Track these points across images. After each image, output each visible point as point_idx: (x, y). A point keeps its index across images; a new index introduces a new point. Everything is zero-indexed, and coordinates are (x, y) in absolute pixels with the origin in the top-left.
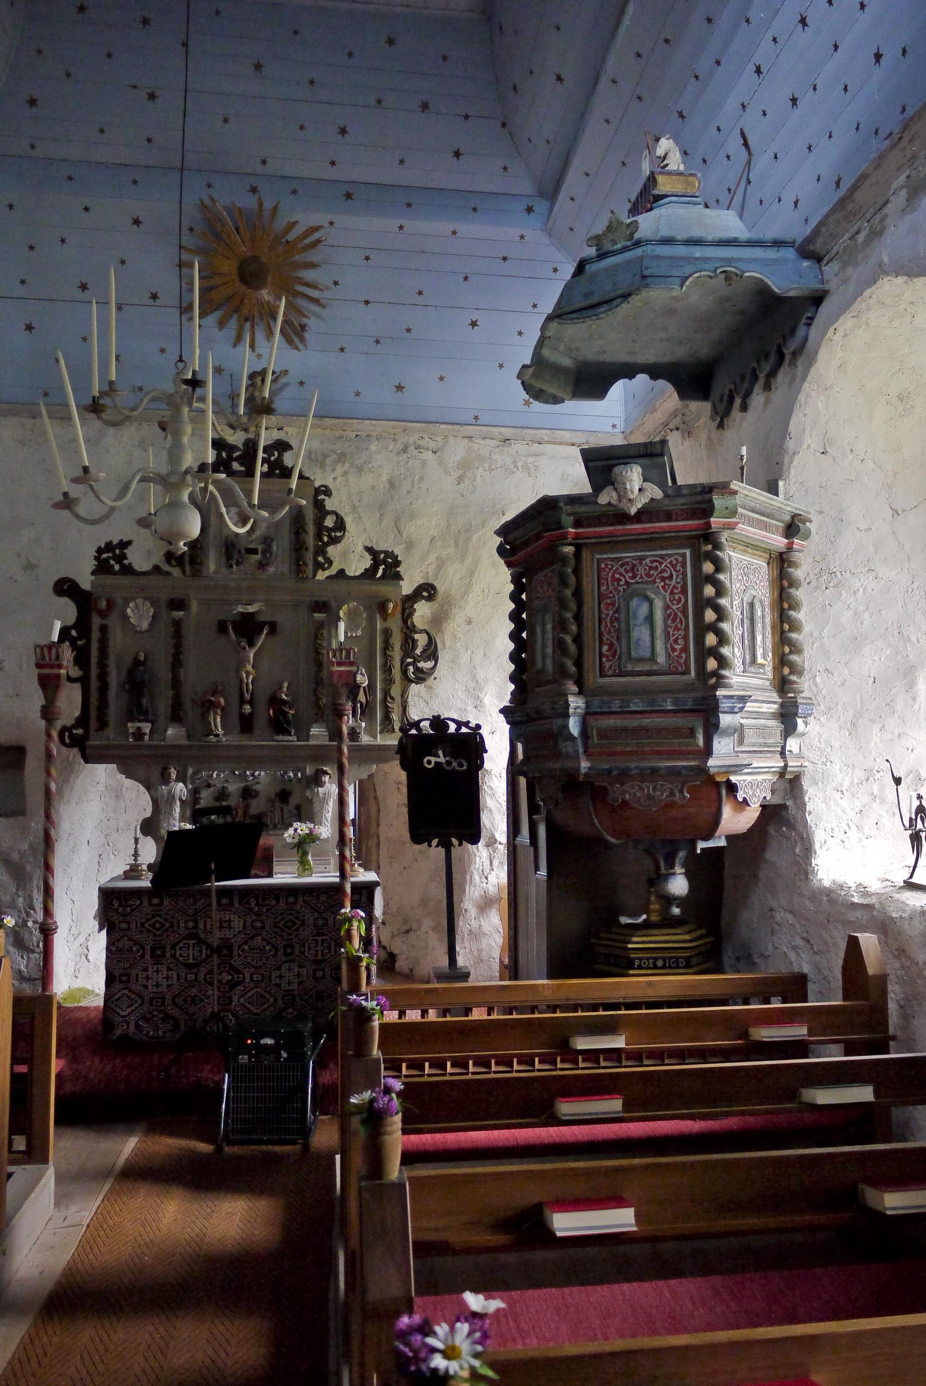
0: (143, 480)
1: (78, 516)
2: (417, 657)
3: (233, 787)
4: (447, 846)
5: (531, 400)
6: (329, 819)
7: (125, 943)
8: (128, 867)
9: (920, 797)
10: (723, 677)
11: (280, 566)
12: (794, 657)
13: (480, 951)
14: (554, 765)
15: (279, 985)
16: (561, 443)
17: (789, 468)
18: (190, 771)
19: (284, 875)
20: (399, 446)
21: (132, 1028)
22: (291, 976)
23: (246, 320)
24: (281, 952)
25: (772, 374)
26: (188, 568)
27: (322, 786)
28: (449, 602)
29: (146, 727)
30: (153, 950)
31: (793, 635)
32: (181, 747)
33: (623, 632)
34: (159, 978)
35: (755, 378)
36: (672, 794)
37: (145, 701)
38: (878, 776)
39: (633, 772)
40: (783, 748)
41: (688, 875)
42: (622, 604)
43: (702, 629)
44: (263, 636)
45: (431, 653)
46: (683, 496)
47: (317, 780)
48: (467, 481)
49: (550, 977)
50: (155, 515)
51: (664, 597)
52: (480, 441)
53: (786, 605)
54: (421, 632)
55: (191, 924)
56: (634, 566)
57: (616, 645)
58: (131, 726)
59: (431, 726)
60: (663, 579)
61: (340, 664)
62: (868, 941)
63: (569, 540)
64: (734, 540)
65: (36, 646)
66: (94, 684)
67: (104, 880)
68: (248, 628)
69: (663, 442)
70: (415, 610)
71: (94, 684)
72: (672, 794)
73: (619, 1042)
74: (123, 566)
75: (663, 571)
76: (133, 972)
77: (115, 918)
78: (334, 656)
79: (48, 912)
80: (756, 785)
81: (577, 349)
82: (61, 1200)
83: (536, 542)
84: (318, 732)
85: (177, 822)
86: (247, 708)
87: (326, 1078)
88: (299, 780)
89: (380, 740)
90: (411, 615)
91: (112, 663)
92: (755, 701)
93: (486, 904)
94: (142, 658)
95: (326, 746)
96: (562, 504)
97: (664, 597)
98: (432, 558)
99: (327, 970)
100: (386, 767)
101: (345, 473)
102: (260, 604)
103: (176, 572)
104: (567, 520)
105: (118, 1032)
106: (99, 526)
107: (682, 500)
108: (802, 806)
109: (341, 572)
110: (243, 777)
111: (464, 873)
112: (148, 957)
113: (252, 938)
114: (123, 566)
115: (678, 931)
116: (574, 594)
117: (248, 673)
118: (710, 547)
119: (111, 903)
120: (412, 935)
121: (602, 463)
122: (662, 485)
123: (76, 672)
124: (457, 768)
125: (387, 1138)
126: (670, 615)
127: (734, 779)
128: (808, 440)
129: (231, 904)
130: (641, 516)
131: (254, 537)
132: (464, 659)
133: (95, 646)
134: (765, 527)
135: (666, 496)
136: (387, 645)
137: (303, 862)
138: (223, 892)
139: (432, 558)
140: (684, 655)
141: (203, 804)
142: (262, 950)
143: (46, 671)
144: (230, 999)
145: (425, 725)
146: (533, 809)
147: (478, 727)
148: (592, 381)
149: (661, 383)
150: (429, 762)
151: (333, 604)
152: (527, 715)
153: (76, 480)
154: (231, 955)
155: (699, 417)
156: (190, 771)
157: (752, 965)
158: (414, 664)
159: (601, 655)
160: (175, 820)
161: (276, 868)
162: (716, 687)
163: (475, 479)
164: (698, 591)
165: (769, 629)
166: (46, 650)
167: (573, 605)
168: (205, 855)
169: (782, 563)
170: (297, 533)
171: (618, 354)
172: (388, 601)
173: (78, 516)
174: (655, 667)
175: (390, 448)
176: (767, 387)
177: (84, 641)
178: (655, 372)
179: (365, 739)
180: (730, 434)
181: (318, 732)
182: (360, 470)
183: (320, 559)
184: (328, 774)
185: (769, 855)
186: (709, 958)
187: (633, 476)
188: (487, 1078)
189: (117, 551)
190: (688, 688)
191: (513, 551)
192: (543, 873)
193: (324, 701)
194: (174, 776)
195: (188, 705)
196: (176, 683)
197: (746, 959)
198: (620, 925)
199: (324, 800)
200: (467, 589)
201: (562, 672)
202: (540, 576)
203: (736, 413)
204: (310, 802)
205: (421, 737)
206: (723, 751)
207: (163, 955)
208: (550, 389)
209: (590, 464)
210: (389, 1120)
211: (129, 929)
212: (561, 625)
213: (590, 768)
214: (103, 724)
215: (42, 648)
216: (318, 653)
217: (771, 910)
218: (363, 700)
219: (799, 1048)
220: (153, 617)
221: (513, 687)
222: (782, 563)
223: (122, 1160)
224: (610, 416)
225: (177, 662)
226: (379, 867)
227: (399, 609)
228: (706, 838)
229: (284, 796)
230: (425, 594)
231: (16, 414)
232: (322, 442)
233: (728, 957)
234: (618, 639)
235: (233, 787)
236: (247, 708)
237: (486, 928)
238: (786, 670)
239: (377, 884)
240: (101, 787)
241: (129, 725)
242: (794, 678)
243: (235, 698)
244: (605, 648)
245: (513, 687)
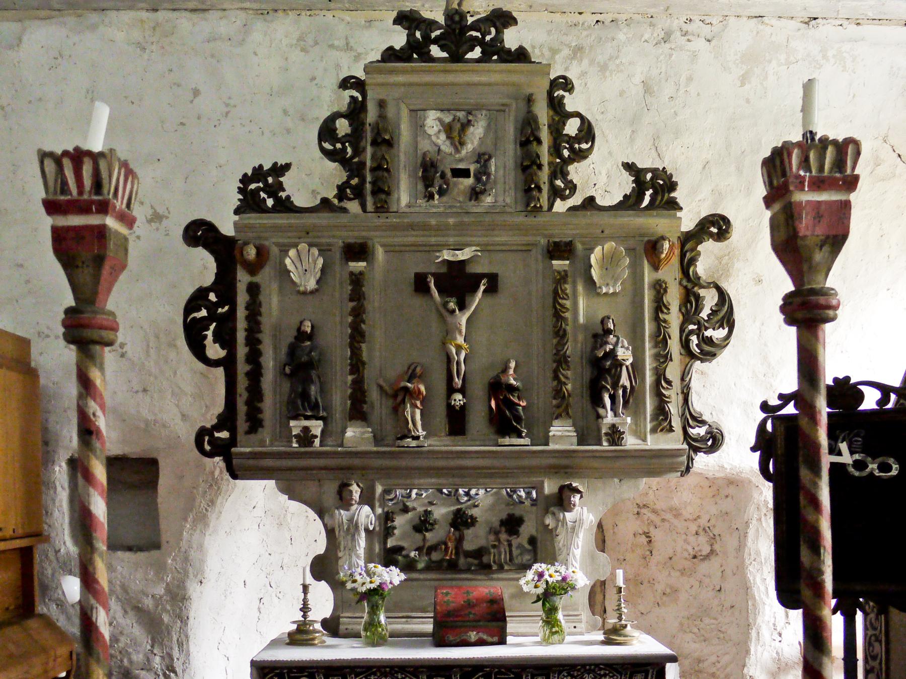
3: (441, 512)
6: (578, 557)
8: (294, 627)
11: (502, 193)
18: (379, 489)
19: (523, 643)
20: (659, 33)
26: (370, 200)
27: (570, 510)
29: (316, 427)
37: (313, 390)
44: (480, 294)
47: (562, 500)
52: (774, 22)
54: (708, 286)
58: (296, 426)
61: (819, 184)
66: (242, 368)
68: (458, 283)
70: (699, 254)
71: (242, 368)
74: (278, 200)
78: (805, 162)
88: (534, 503)
90: (693, 261)
94: (309, 330)
95: (574, 451)
102: (474, 248)
109: (590, 202)
114: (278, 200)
124: (877, 473)
131: (464, 152)
133: (241, 313)
136: (660, 306)
137: (550, 621)
143: (76, 220)
151: (579, 247)
156: (379, 489)
158: (698, 332)
160: (358, 557)
163: (766, 78)
166: (67, 163)
172: (663, 238)
175: (646, 36)
177: (226, 308)
179: (631, 442)
181: (562, 434)
182: (604, 68)
183: (559, 183)
184: (579, 492)
189: (270, 180)
193: (569, 387)
194: (356, 496)
195: (374, 395)
196: (357, 365)
204: (551, 533)
214: (255, 424)
215: (58, 160)
216: (558, 315)
220: (323, 270)
225: (357, 336)
226: (605, 611)
227: (677, 251)
229: (512, 524)
230: (714, 230)
232: (549, 32)
236: (458, 399)
240: (259, 512)
241: (292, 423)
243: (441, 387)
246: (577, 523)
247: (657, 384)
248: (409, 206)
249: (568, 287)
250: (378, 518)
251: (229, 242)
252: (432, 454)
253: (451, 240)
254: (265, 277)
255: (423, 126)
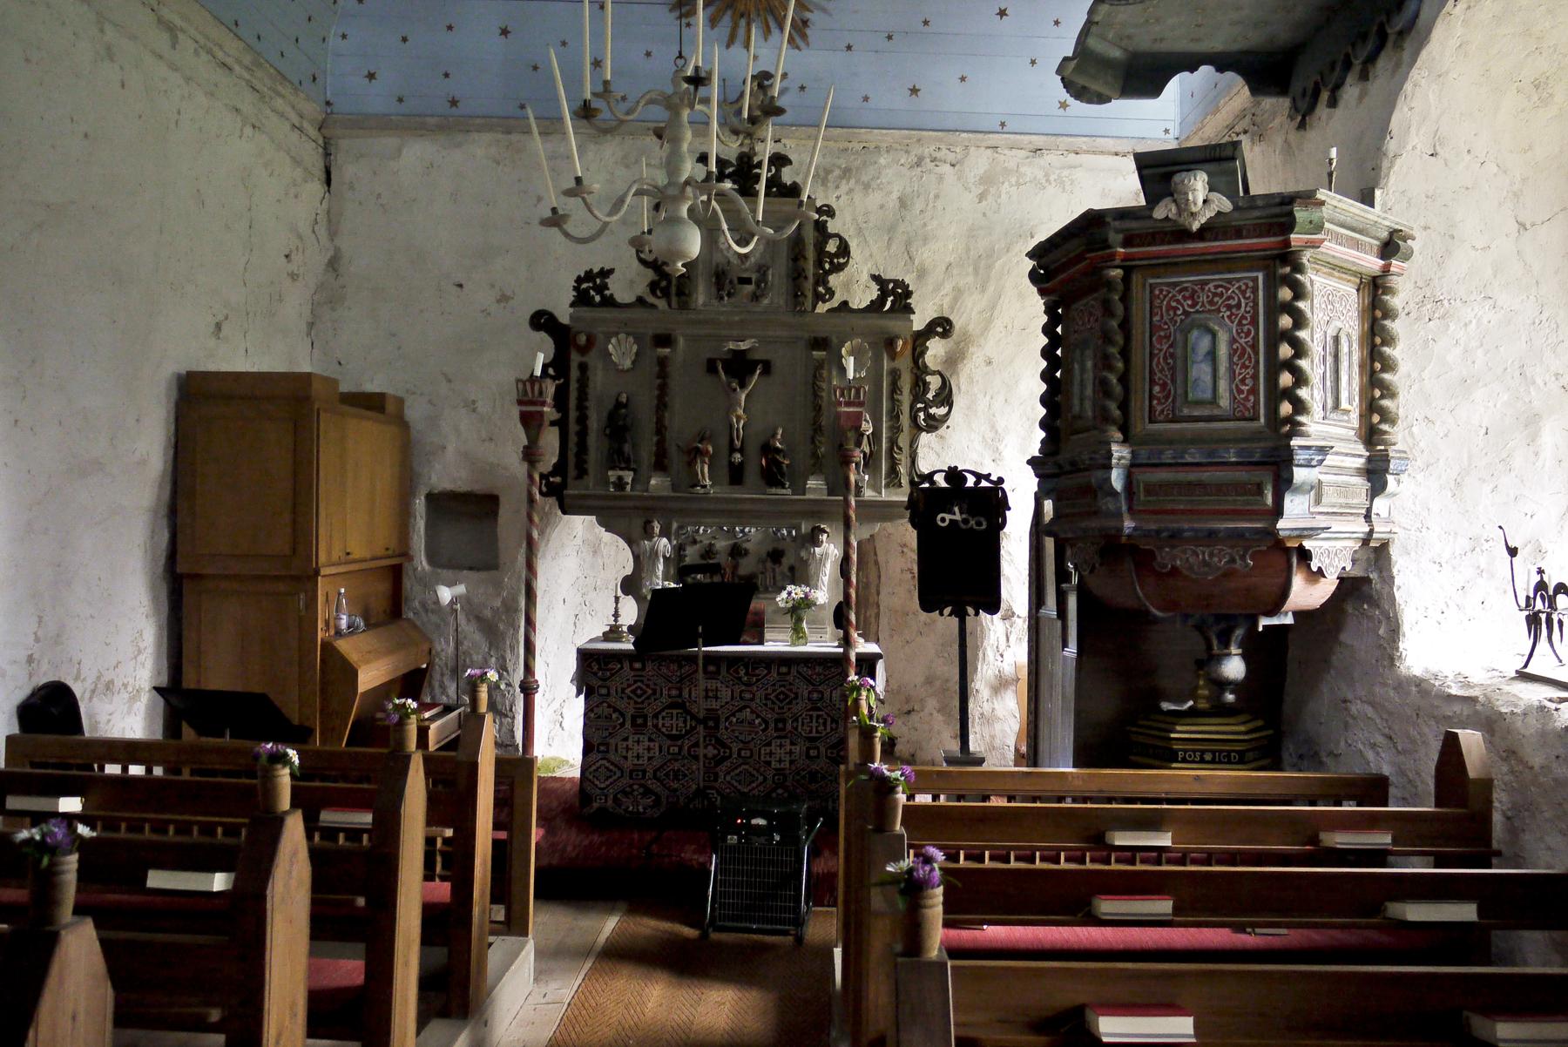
0: (639, 193)
1: (567, 235)
2: (929, 401)
3: (722, 544)
4: (961, 615)
5: (1071, 100)
7: (604, 710)
9: (1541, 572)
10: (1301, 424)
11: (776, 297)
12: (1386, 403)
13: (993, 737)
14: (1094, 523)
15: (769, 763)
16: (1102, 153)
17: (1388, 175)
18: (675, 525)
19: (776, 643)
21: (610, 802)
22: (782, 754)
23: (742, 16)
24: (772, 725)
25: (1372, 59)
26: (674, 300)
28: (967, 339)
29: (628, 477)
30: (634, 718)
31: (1386, 376)
32: (667, 499)
33: (1178, 366)
34: (639, 750)
35: (1348, 65)
36: (1233, 560)
37: (627, 448)
38: (1486, 546)
39: (1186, 534)
40: (1369, 510)
41: (1246, 657)
42: (1179, 337)
43: (1276, 366)
45: (946, 397)
46: (1257, 208)
47: (813, 539)
48: (990, 198)
49: (1074, 766)
50: (650, 232)
51: (1230, 331)
53: (1378, 340)
54: (934, 373)
55: (674, 692)
56: (1194, 292)
57: (1170, 386)
58: (613, 475)
59: (947, 479)
60: (1229, 307)
61: (848, 404)
62: (1471, 740)
63: (1117, 262)
64: (1316, 261)
65: (518, 381)
66: (573, 427)
67: (582, 641)
68: (740, 367)
69: (1236, 145)
71: (573, 427)
72: (1233, 560)
73: (1164, 840)
75: (1229, 298)
76: (612, 741)
77: (595, 682)
78: (842, 395)
79: (529, 670)
80: (1334, 555)
81: (1129, 37)
82: (540, 975)
83: (1076, 266)
84: (815, 485)
85: (659, 579)
86: (737, 457)
87: (821, 866)
88: (794, 539)
89: (886, 495)
90: (923, 353)
91: (591, 404)
92: (1337, 454)
93: (1001, 684)
96: (1108, 219)
97: (1230, 331)
98: (948, 287)
99: (823, 750)
100: (889, 526)
101: (851, 191)
103: (661, 304)
104: (1114, 238)
105: (596, 805)
106: (591, 245)
107: (1257, 213)
108: (1389, 580)
109: (845, 303)
110: (732, 532)
111: (977, 648)
112: (628, 725)
113: (740, 710)
115: (1232, 720)
116: (1120, 326)
117: (739, 418)
118: (1288, 269)
119: (589, 666)
120: (914, 717)
121: (1159, 171)
122: (1232, 196)
123: (555, 416)
125: (928, 912)
126: (1235, 351)
127: (1307, 544)
128: (1414, 139)
129: (718, 672)
130: (1206, 232)
132: (982, 404)
133: (573, 386)
134: (1357, 245)
135: (1236, 208)
136: (895, 388)
137: (797, 630)
138: (710, 658)
139: (948, 287)
140: (1252, 398)
141: (688, 561)
142: (751, 723)
144: (716, 776)
145: (940, 480)
146: (1062, 576)
147: (1001, 480)
148: (1144, 76)
149: (1230, 75)
150: (943, 520)
151: (835, 340)
152: (1060, 467)
153: (569, 193)
154: (717, 727)
155: (1274, 115)
156: (675, 525)
157: (1319, 765)
158: (925, 410)
159: (1151, 397)
161: (767, 636)
162: (1290, 436)
164: (1272, 322)
165: (1356, 369)
167: (1119, 339)
168: (690, 616)
169: (1375, 290)
170: (795, 260)
171: (1178, 42)
172: (898, 337)
173: (567, 235)
174: (1216, 412)
176: (1364, 76)
178: (1222, 63)
180: (1312, 135)
181: (815, 485)
182: (867, 186)
183: (821, 289)
185: (1343, 637)
186: (1267, 753)
187: (1198, 185)
188: (1026, 862)
190: (1255, 436)
191: (1049, 276)
192: (1072, 650)
194: (657, 530)
195: (672, 450)
196: (660, 429)
197: (1311, 756)
198: (1162, 712)
199: (821, 561)
200: (987, 324)
201: (1106, 418)
202: (1079, 305)
203: (1322, 110)
204: (805, 563)
205: (935, 491)
206: (1295, 512)
207: (645, 724)
208: (1095, 86)
209: (1145, 172)
210: (930, 891)
211: (608, 694)
212: (1105, 362)
213: (1135, 529)
214: (582, 472)
215: (524, 383)
216: (816, 395)
217: (1345, 701)
218: (867, 450)
219: (1377, 856)
220: (637, 354)
221: (1043, 434)
222: (1375, 290)
223: (602, 938)
224: (1164, 117)
225: (662, 405)
227: (909, 347)
228: (1270, 614)
229: (776, 556)
230: (940, 330)
231: (490, 128)
233: (1289, 750)
234: (1173, 381)
235: (722, 544)
236: (737, 457)
237: (1000, 712)
238: (1376, 418)
239: (879, 656)
240: (578, 541)
242: (1385, 427)
243: (725, 450)
244: (1157, 389)
245: (1043, 434)
246: (825, 556)
247: (890, 451)
248: (704, 305)
249: (825, 373)
250: (673, 548)
251: (566, 328)
252: (717, 500)
253: (735, 333)
254: (592, 359)
255: (716, 242)
